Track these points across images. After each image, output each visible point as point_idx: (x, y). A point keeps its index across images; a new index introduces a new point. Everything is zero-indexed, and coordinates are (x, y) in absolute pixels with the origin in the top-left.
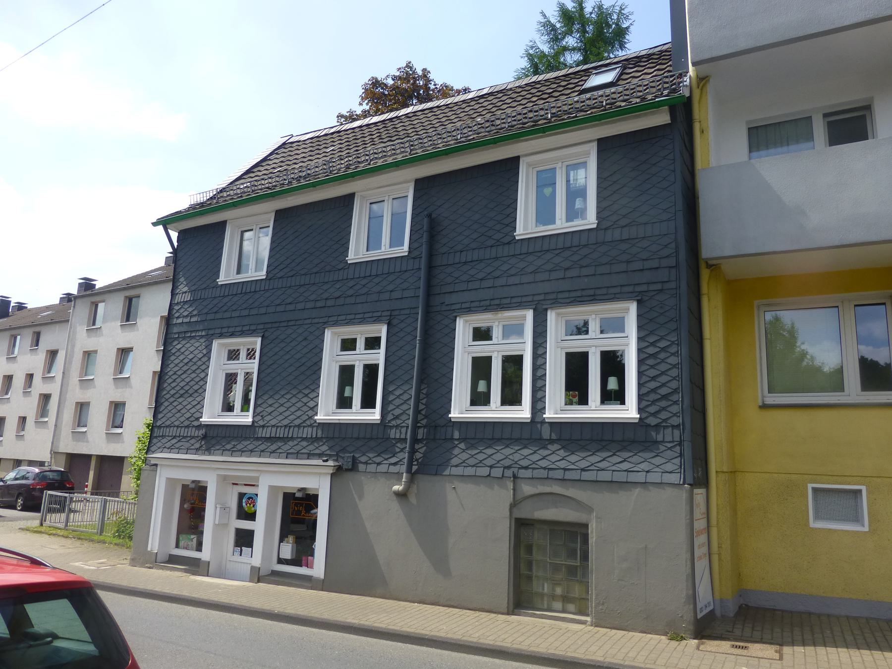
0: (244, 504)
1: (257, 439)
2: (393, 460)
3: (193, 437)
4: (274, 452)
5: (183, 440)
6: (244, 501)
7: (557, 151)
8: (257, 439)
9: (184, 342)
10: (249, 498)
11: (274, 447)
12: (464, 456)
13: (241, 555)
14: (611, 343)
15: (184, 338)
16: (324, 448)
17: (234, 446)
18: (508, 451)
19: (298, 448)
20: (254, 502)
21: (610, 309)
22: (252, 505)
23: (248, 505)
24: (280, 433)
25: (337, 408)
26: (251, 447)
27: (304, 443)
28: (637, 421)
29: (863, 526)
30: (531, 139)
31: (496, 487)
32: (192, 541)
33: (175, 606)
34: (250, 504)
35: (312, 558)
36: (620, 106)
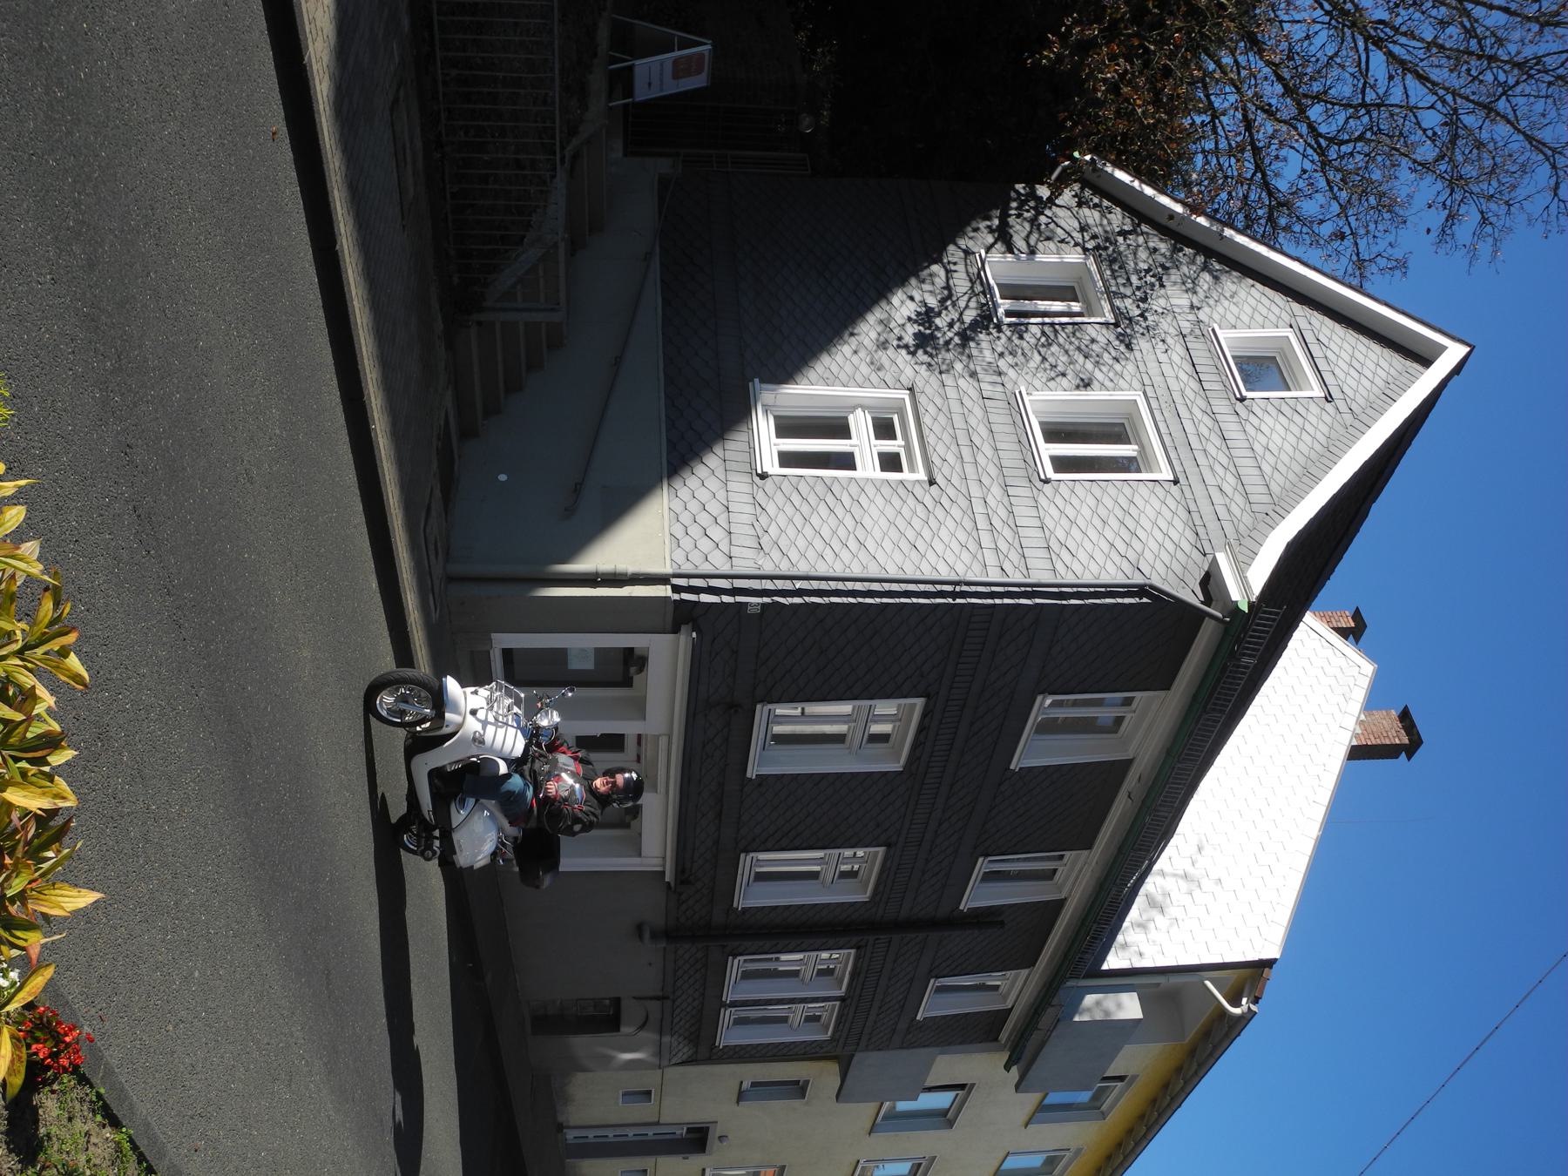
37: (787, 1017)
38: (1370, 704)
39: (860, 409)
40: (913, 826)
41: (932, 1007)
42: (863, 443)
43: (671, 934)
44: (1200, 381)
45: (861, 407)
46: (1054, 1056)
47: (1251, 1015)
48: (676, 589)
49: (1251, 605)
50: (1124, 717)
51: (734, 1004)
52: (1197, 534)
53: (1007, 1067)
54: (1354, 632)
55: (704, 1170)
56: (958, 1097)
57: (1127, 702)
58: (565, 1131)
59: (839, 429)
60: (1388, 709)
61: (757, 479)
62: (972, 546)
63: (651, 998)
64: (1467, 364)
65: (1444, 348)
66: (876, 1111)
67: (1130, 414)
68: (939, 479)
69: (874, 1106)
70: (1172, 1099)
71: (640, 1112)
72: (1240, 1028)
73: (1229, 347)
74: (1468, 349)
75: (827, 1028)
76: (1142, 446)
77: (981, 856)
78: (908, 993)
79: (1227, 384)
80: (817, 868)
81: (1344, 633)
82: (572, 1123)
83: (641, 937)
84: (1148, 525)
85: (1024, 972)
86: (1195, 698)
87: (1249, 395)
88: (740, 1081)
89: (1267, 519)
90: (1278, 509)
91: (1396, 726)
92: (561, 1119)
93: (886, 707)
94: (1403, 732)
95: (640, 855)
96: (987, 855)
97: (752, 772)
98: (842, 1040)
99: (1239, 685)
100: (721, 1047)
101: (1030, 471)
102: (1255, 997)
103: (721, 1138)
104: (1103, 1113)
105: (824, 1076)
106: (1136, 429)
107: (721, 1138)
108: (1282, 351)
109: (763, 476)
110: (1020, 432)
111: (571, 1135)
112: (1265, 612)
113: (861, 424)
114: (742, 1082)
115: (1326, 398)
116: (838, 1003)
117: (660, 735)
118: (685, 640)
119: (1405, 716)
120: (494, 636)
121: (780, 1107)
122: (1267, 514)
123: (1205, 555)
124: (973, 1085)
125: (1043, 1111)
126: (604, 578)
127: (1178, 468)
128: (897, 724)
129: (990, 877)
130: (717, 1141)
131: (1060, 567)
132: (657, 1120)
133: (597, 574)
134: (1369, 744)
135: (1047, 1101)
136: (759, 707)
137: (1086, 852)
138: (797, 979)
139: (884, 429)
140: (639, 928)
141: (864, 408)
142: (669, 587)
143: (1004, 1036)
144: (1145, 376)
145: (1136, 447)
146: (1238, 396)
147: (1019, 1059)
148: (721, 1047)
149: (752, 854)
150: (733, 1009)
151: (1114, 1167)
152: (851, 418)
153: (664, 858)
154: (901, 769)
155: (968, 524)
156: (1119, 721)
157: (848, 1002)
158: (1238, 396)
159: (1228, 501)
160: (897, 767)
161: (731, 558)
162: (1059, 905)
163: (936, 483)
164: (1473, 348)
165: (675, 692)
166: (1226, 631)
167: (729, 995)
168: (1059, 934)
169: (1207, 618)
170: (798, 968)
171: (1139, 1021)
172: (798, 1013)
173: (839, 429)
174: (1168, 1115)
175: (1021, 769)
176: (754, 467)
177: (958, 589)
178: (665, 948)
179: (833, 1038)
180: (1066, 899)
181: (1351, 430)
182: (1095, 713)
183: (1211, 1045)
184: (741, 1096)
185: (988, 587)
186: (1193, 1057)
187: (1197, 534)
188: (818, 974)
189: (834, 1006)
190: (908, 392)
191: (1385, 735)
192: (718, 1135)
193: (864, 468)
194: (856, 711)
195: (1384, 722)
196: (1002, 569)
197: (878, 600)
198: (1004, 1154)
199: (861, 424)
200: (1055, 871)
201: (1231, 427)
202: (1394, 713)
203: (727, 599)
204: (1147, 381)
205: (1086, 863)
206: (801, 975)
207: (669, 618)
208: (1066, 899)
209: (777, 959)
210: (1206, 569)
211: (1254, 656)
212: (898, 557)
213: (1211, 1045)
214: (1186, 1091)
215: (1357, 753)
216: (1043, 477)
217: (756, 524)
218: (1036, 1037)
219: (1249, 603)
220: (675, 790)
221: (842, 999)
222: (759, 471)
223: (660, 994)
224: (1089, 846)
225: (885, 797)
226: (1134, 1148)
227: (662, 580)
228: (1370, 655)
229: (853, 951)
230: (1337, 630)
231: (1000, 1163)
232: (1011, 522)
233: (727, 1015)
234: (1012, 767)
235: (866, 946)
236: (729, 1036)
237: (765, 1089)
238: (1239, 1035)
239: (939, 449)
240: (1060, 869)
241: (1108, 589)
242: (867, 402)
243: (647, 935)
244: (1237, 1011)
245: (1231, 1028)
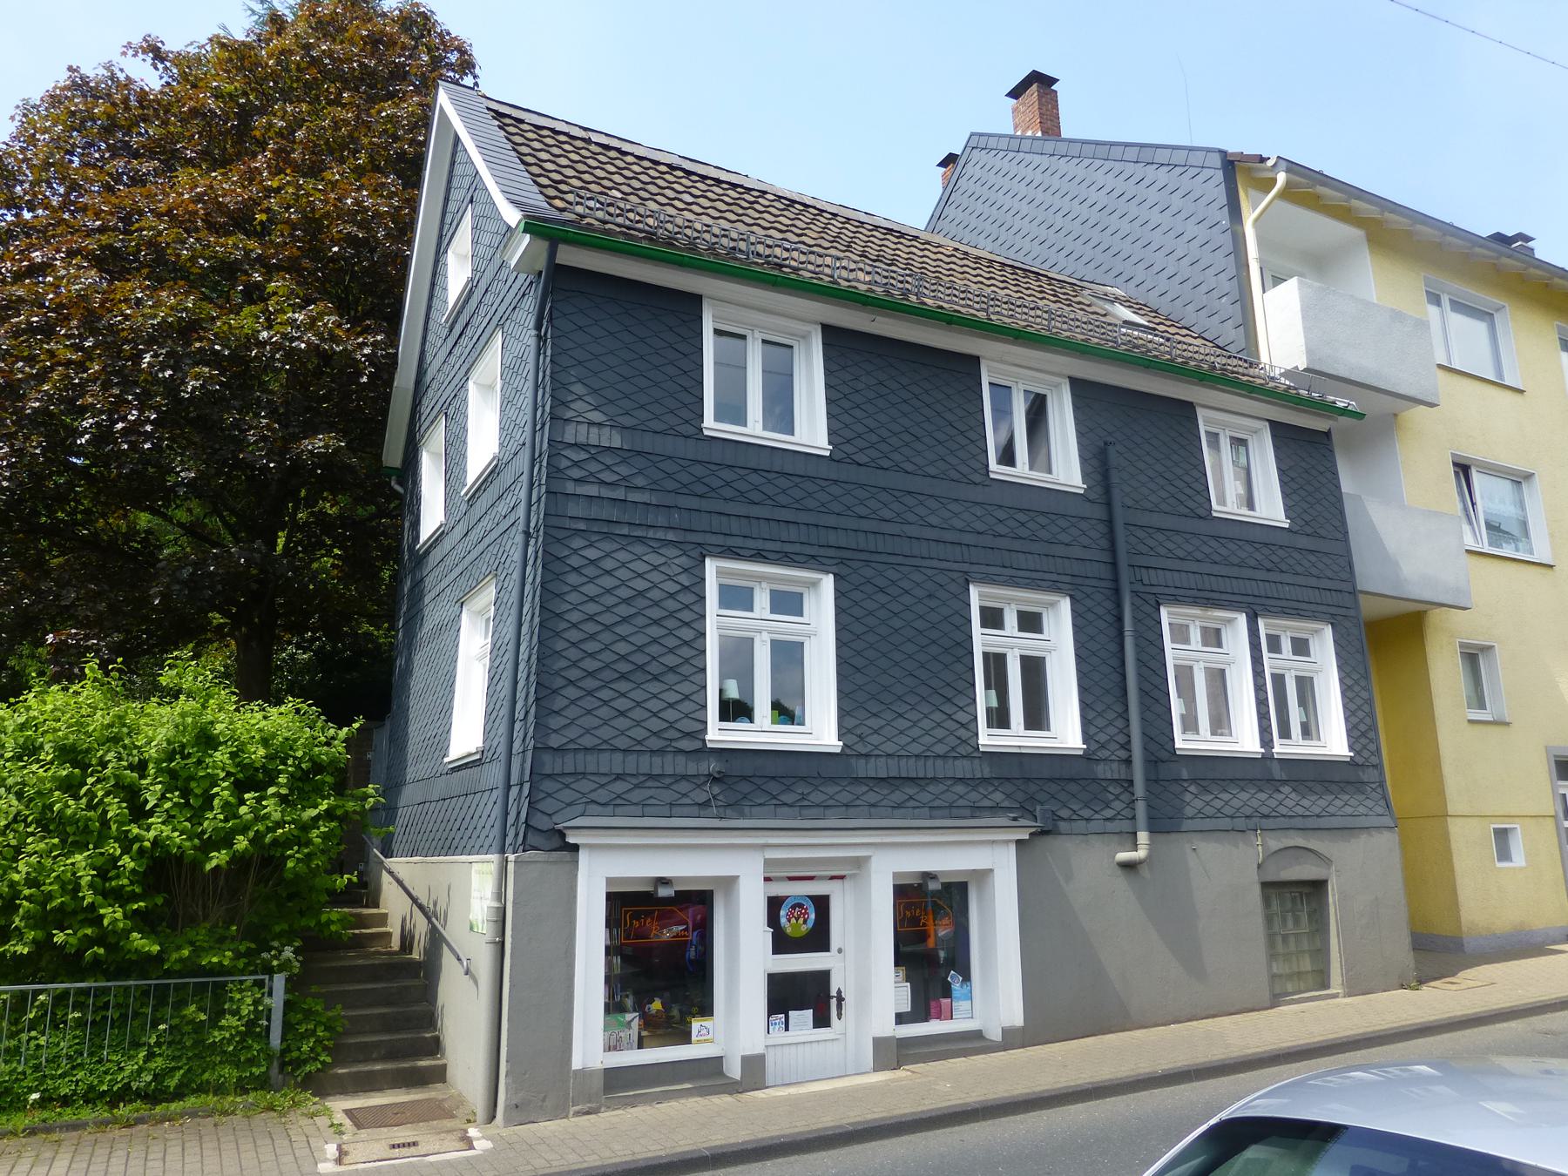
0: (783, 920)
1: (857, 780)
2: (1109, 813)
3: (684, 777)
4: (899, 806)
5: (647, 784)
6: (782, 913)
7: (1235, 417)
8: (857, 780)
9: (608, 546)
10: (794, 907)
11: (897, 797)
12: (1198, 804)
13: (787, 1029)
14: (1030, 644)
15: (607, 536)
16: (998, 797)
17: (804, 797)
18: (1244, 796)
19: (949, 797)
20: (804, 914)
21: (1031, 599)
22: (801, 921)
23: (793, 921)
24: (909, 768)
25: (772, 723)
26: (845, 797)
27: (960, 789)
28: (1081, 753)
29: (984, 875)
30: (1228, 392)
31: (1241, 845)
32: (630, 1028)
33: (857, 1149)
34: (797, 919)
35: (949, 1000)
36: (925, 304)
180: (1070, 378)
208: (1070, 378)
233: (1280, 748)
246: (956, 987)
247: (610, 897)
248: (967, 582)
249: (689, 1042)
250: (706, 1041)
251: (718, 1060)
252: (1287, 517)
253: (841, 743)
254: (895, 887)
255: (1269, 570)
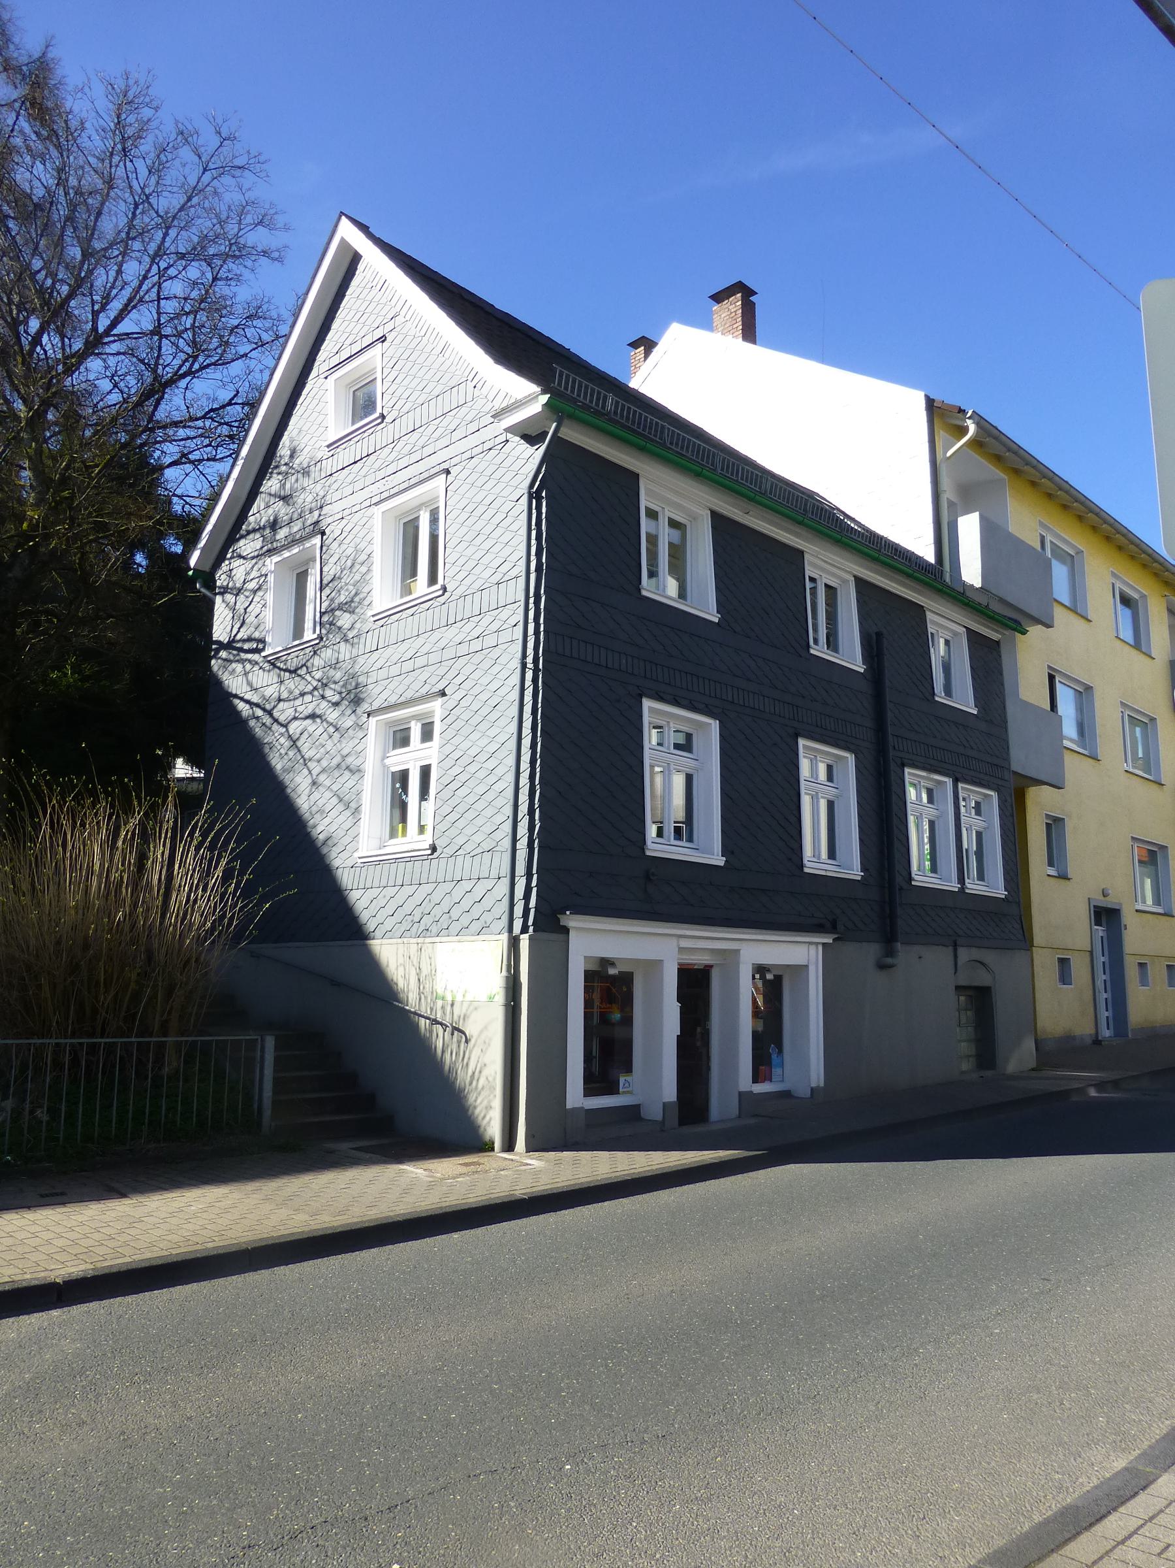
37: (976, 832)
38: (707, 324)
39: (385, 761)
40: (777, 712)
41: (964, 700)
42: (411, 758)
43: (889, 938)
44: (368, 455)
45: (383, 759)
46: (1018, 595)
47: (976, 416)
48: (524, 930)
49: (544, 392)
50: (669, 519)
51: (961, 880)
52: (490, 449)
53: (1024, 632)
54: (647, 344)
55: (1137, 911)
56: (827, 577)
57: (652, 515)
58: (1100, 1038)
59: (402, 777)
60: (711, 313)
61: (436, 855)
62: (496, 652)
63: (956, 956)
64: (502, 303)
65: (343, 240)
66: (1076, 754)
67: (396, 517)
68: (440, 686)
69: (1068, 757)
70: (1044, 477)
71: (1080, 968)
72: (988, 426)
73: (344, 429)
74: (343, 217)
75: (986, 796)
76: (419, 508)
77: (808, 651)
78: (644, 618)
79: (371, 431)
80: (823, 805)
81: (647, 354)
82: (1093, 1032)
83: (891, 966)
84: (482, 494)
85: (929, 615)
86: (641, 449)
87: (379, 410)
88: (1048, 878)
89: (479, 386)
90: (470, 378)
91: (727, 306)
92: (1089, 1041)
93: (911, 793)
94: (731, 299)
95: (807, 966)
96: (808, 646)
97: (720, 861)
98: (1000, 782)
99: (635, 412)
100: (1006, 893)
101: (436, 604)
102: (959, 412)
103: (1105, 894)
104: (1077, 553)
105: (1040, 802)
106: (407, 512)
107: (1105, 894)
108: (349, 386)
109: (434, 849)
110: (404, 614)
111: (1106, 1033)
112: (560, 384)
113: (400, 759)
114: (1049, 875)
115: (383, 342)
116: (960, 785)
117: (678, 945)
118: (572, 921)
119: (718, 298)
120: (569, 1105)
121: (1073, 843)
122: (475, 387)
123: (507, 441)
124: (1049, 667)
125: (1077, 609)
126: (510, 998)
127: (437, 469)
128: (818, 758)
129: (832, 642)
130: (1107, 898)
131: (513, 573)
132: (1088, 953)
133: (507, 1005)
134: (741, 327)
135: (1066, 600)
136: (648, 853)
137: (806, 556)
138: (936, 823)
139: (402, 739)
140: (882, 967)
141: (384, 757)
142: (522, 936)
143: (995, 636)
144: (363, 505)
145: (422, 513)
146: (379, 420)
147: (1016, 621)
148: (1006, 893)
149: (913, 875)
150: (967, 881)
151: (1101, 521)
152: (394, 769)
153: (810, 943)
154: (718, 722)
155: (478, 658)
156: (673, 524)
157: (959, 776)
158: (379, 420)
159: (464, 423)
160: (714, 725)
161: (499, 878)
162: (860, 582)
163: (443, 690)
164: (342, 213)
165: (621, 931)
166: (571, 417)
167: (954, 886)
168: (588, 440)
169: (559, 435)
170: (974, 832)
171: (982, 518)
172: (970, 819)
173: (402, 777)
174: (1075, 492)
175: (718, 612)
176: (426, 857)
177: (530, 665)
178: (901, 943)
179: (997, 789)
180: (855, 577)
181: (408, 318)
182: (664, 543)
183: (1007, 454)
184: (1064, 877)
185: (529, 639)
186: (1069, 507)
187: (490, 449)
188: (980, 815)
189: (909, 774)
190: (370, 718)
191: (734, 314)
192: (1101, 898)
193: (430, 757)
194: (661, 764)
195: (723, 316)
196: (515, 626)
197: (539, 739)
198: (1119, 642)
199: (400, 759)
200: (826, 585)
201: (406, 424)
202: (716, 307)
203: (534, 883)
204: (367, 503)
205: (817, 557)
206: (981, 830)
207: (553, 936)
208: (855, 577)
209: (967, 850)
210: (519, 439)
211: (605, 397)
212: (503, 722)
213: (1104, 526)
214: (1098, 512)
215: (749, 333)
216: (440, 592)
217: (472, 854)
218: (996, 607)
219: (542, 394)
220: (735, 933)
221: (956, 781)
222: (429, 852)
223: (951, 948)
224: (802, 553)
225: (761, 741)
226: (1108, 524)
227: (514, 943)
228: (663, 327)
229: (907, 770)
230: (646, 357)
231: (1126, 645)
232: (476, 619)
233: (974, 886)
234: (716, 620)
235: (901, 758)
236: (995, 887)
237: (1055, 854)
238: (1067, 482)
239: (416, 687)
240: (825, 581)
241: (533, 527)
242: (379, 755)
243: (889, 960)
244: (972, 428)
245: (990, 435)
246: (774, 1056)
247: (679, 970)
248: (641, 696)
249: (618, 1093)
250: (628, 1092)
251: (637, 1108)
252: (976, 706)
253: (724, 859)
254: (586, 972)
255: (749, 680)
